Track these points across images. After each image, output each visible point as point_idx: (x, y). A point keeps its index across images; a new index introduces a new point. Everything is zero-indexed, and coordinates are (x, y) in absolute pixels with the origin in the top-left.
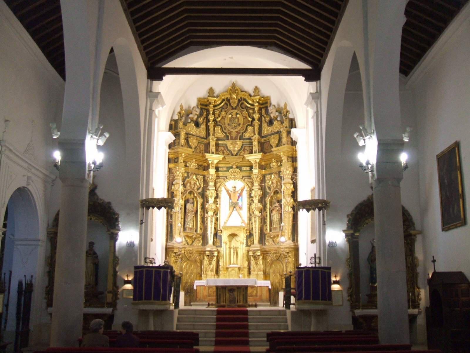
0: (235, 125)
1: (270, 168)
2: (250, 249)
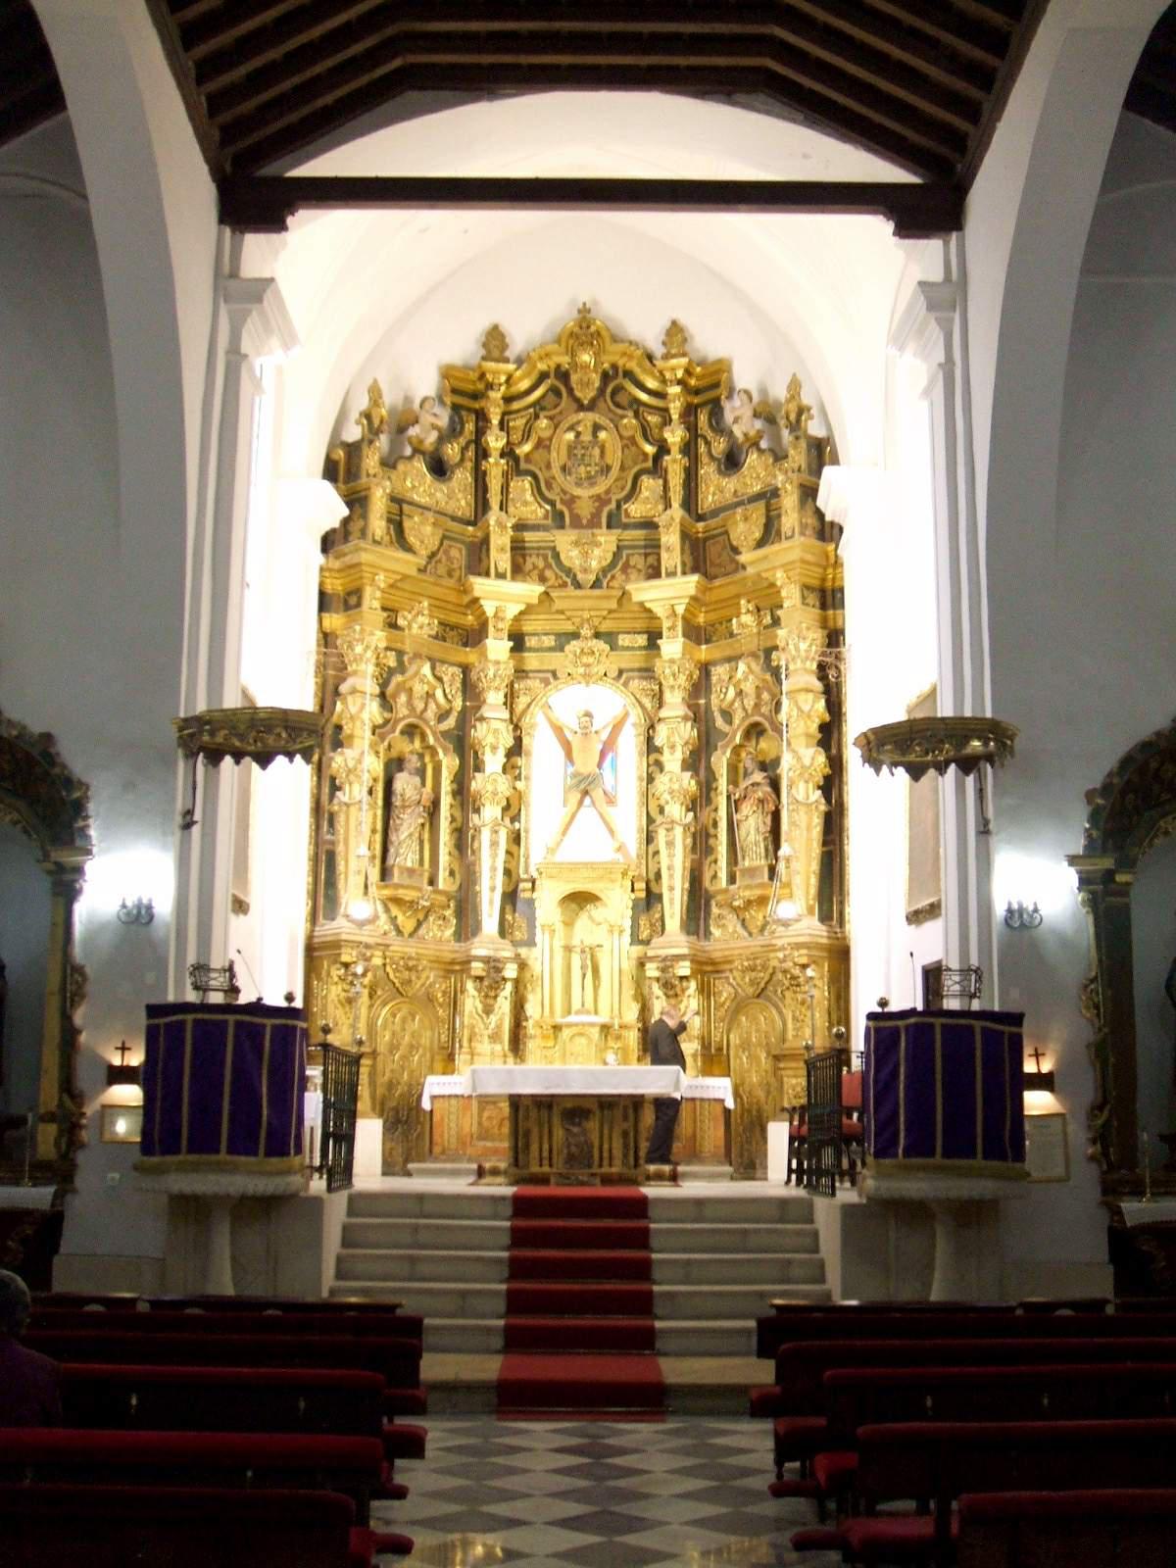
0: (589, 472)
1: (732, 635)
2: (650, 953)
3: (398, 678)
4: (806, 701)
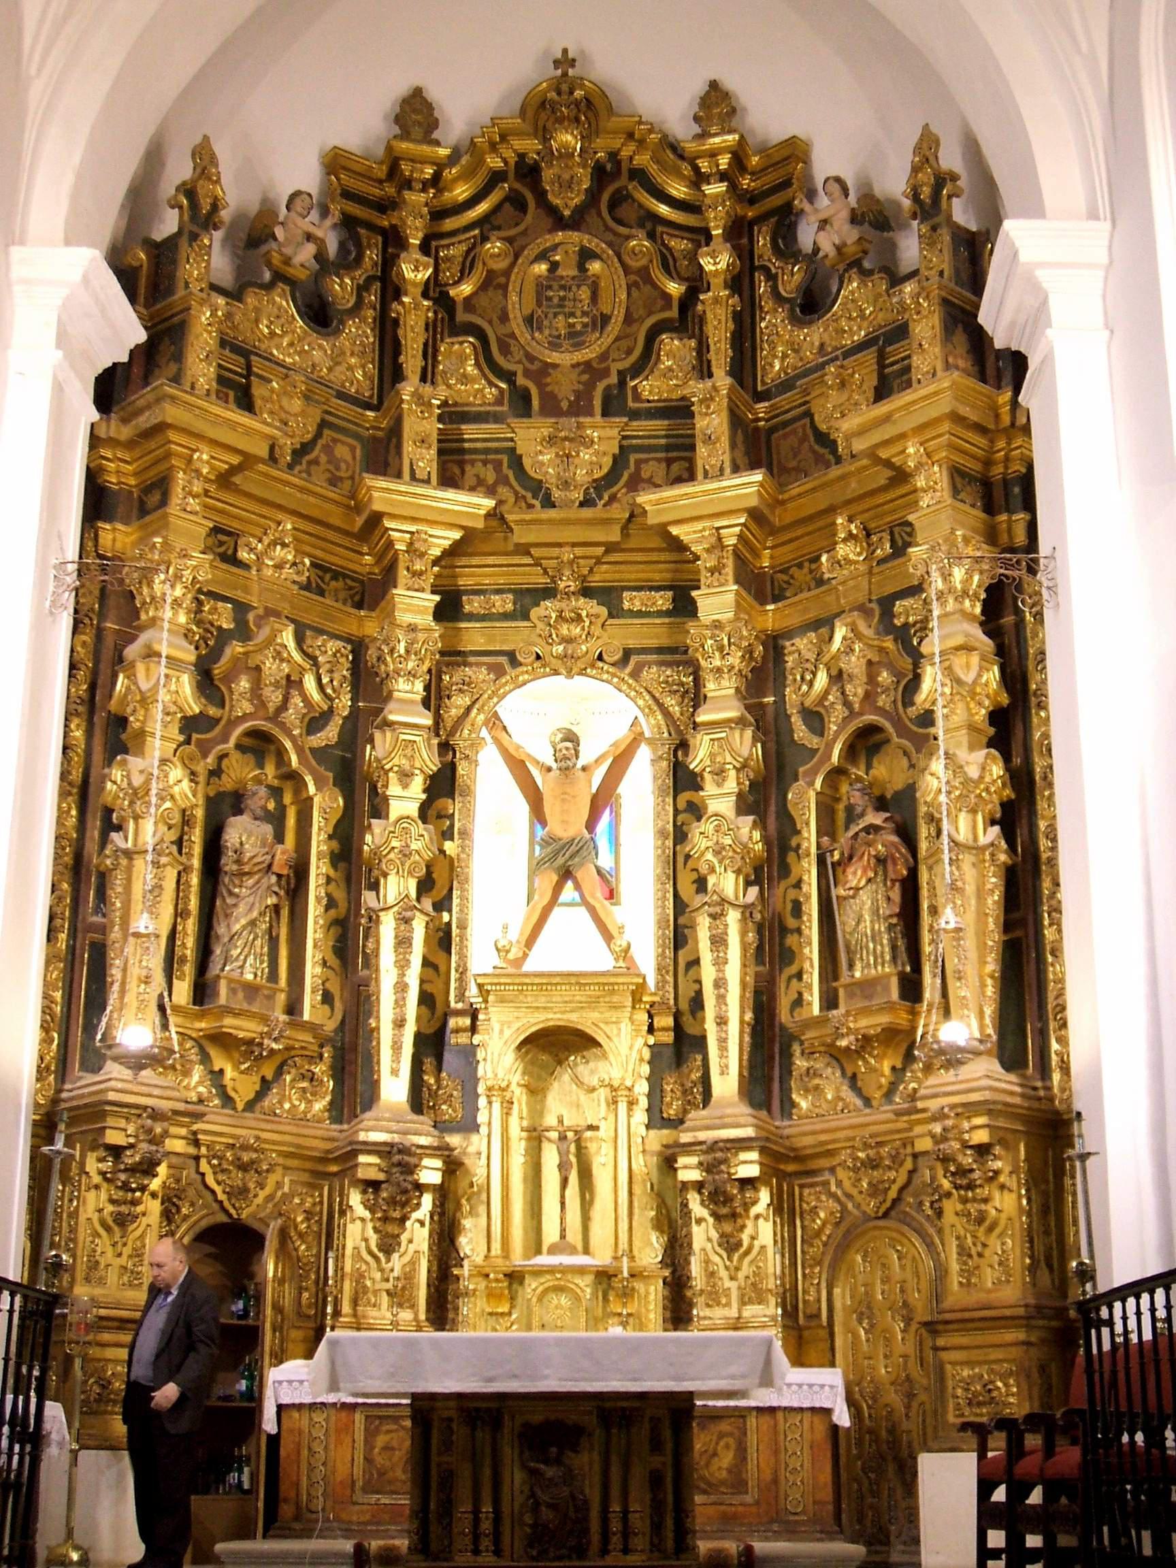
0: (572, 326)
1: (820, 582)
2: (685, 1138)
3: (236, 648)
4: (968, 666)
